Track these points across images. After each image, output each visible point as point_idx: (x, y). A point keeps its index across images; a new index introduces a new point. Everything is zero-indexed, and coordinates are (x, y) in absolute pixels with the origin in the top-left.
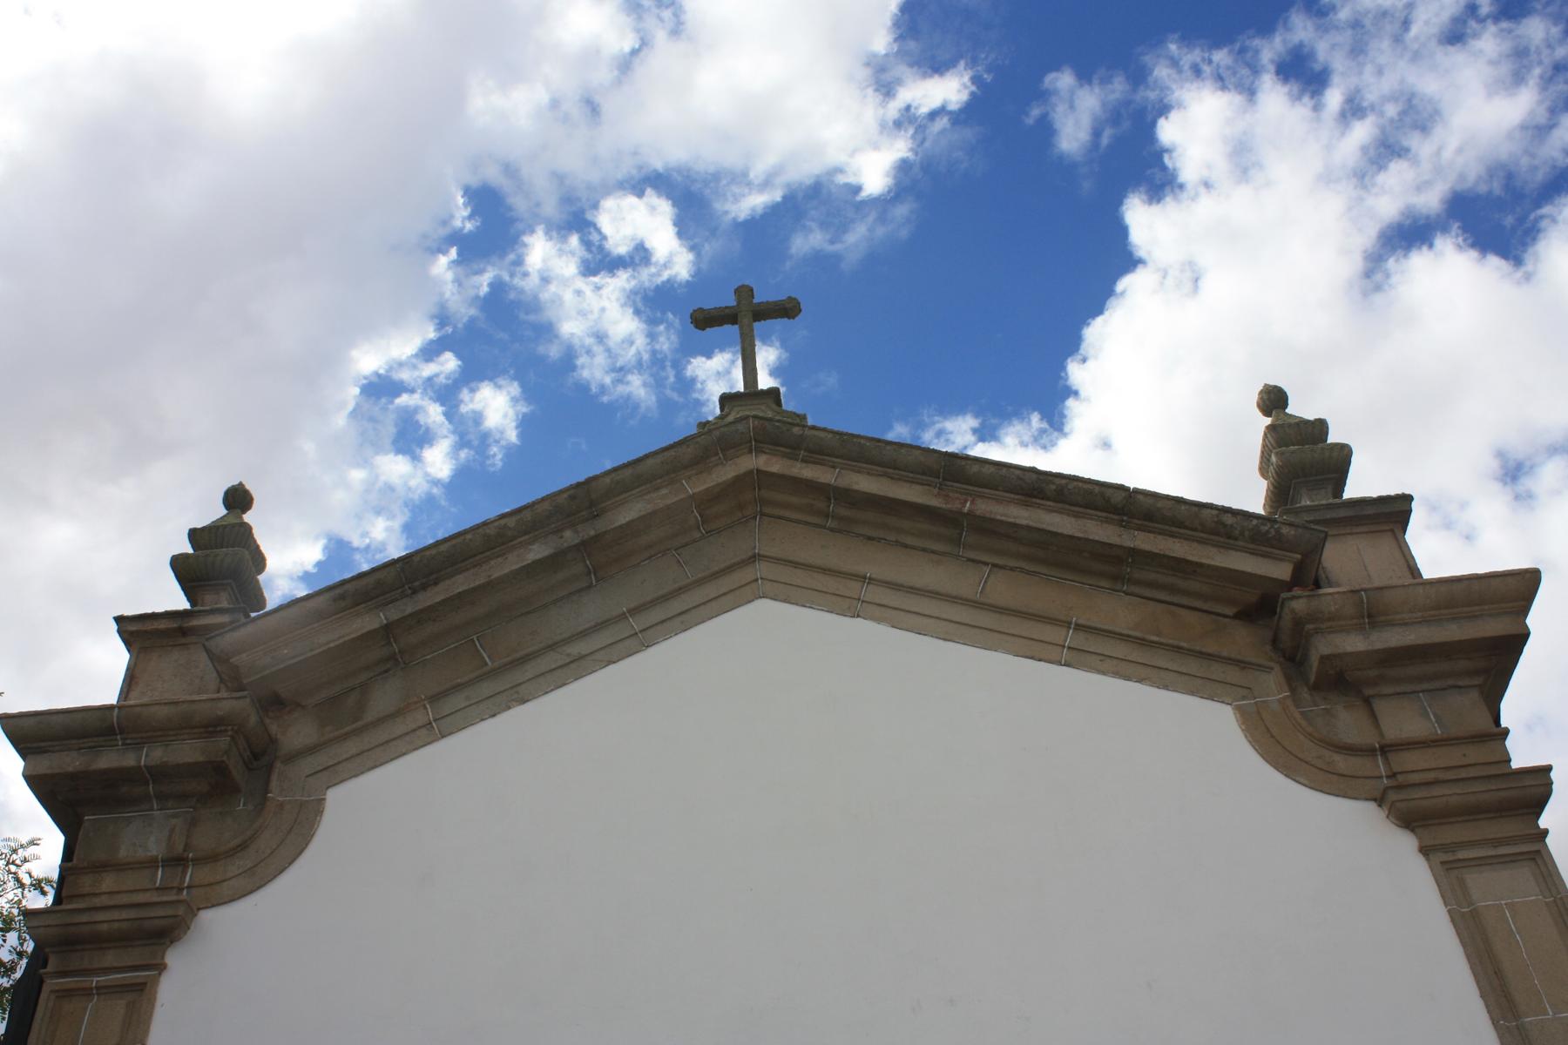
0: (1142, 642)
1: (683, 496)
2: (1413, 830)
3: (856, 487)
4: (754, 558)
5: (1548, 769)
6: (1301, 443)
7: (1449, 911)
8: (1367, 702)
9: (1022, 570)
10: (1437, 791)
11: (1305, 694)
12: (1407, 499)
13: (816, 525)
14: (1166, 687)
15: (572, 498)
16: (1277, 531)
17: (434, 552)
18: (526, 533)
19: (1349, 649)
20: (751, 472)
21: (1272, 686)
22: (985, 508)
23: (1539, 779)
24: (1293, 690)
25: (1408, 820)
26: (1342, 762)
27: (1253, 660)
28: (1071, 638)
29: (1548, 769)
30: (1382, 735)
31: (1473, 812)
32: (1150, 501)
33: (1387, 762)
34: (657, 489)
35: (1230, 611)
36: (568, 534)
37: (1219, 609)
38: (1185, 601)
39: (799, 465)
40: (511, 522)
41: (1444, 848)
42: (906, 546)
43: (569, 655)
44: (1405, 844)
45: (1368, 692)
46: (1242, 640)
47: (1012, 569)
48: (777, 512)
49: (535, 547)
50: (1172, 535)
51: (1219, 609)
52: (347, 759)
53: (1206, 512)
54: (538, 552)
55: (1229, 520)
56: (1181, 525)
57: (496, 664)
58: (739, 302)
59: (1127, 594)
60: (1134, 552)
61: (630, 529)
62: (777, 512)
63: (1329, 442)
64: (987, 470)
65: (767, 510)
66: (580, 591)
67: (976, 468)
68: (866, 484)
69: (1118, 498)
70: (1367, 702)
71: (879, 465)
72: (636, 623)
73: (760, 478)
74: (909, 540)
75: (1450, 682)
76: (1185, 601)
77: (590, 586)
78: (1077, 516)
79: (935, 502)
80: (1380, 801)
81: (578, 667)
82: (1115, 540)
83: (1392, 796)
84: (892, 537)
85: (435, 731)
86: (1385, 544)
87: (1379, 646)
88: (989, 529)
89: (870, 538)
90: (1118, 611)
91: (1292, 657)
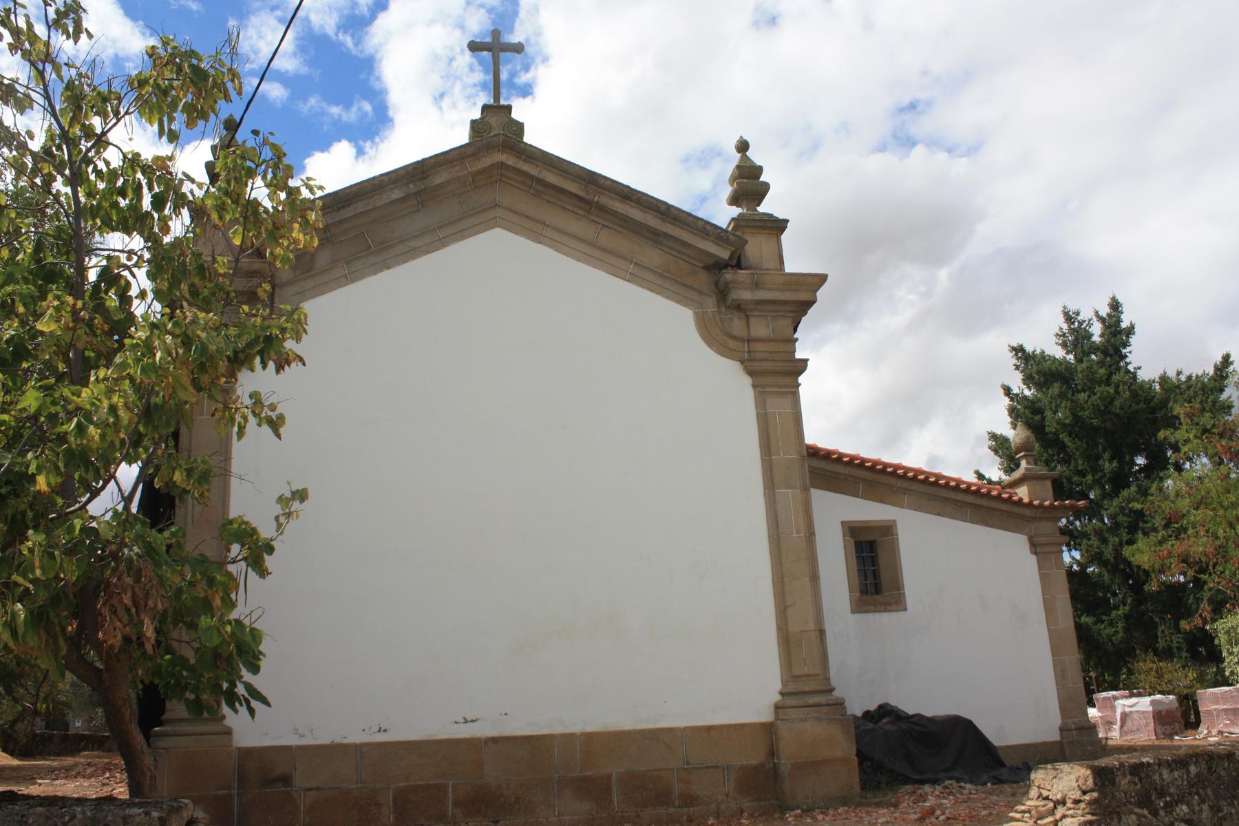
0: (661, 275)
1: (465, 172)
2: (751, 376)
3: (547, 179)
4: (496, 206)
5: (808, 360)
6: (748, 178)
7: (757, 412)
8: (747, 317)
9: (615, 230)
10: (764, 363)
11: (723, 309)
12: (786, 221)
13: (525, 191)
14: (668, 298)
15: (415, 168)
16: (728, 237)
17: (349, 191)
18: (392, 184)
19: (744, 297)
20: (498, 163)
21: (710, 304)
22: (604, 200)
23: (802, 365)
24: (719, 307)
25: (751, 373)
26: (731, 343)
27: (705, 291)
28: (631, 268)
29: (808, 360)
30: (749, 332)
31: (775, 373)
32: (677, 212)
33: (748, 346)
34: (454, 166)
35: (701, 265)
36: (411, 186)
37: (696, 263)
38: (682, 257)
39: (521, 162)
40: (386, 179)
41: (763, 386)
42: (565, 208)
43: (409, 246)
44: (748, 381)
45: (749, 313)
46: (703, 279)
47: (611, 228)
48: (508, 181)
49: (396, 191)
50: (683, 228)
51: (696, 263)
52: (309, 289)
53: (700, 222)
54: (397, 194)
55: (708, 227)
56: (687, 225)
57: (376, 248)
58: (493, 40)
59: (659, 249)
60: (666, 235)
61: (440, 186)
62: (508, 181)
63: (761, 180)
64: (608, 183)
65: (503, 179)
66: (413, 212)
67: (603, 181)
68: (551, 178)
69: (663, 208)
70: (747, 317)
71: (559, 170)
72: (440, 234)
73: (502, 165)
74: (567, 206)
75: (782, 314)
76: (682, 257)
77: (418, 210)
78: (644, 212)
79: (582, 194)
80: (742, 362)
81: (413, 253)
82: (659, 227)
83: (747, 363)
84: (559, 203)
85: (350, 278)
86: (773, 241)
87: (757, 298)
88: (602, 209)
89: (549, 202)
90: (653, 256)
91: (722, 293)
